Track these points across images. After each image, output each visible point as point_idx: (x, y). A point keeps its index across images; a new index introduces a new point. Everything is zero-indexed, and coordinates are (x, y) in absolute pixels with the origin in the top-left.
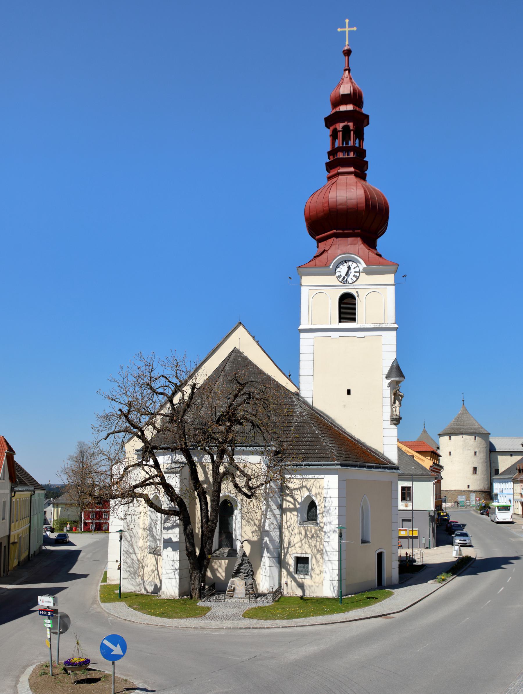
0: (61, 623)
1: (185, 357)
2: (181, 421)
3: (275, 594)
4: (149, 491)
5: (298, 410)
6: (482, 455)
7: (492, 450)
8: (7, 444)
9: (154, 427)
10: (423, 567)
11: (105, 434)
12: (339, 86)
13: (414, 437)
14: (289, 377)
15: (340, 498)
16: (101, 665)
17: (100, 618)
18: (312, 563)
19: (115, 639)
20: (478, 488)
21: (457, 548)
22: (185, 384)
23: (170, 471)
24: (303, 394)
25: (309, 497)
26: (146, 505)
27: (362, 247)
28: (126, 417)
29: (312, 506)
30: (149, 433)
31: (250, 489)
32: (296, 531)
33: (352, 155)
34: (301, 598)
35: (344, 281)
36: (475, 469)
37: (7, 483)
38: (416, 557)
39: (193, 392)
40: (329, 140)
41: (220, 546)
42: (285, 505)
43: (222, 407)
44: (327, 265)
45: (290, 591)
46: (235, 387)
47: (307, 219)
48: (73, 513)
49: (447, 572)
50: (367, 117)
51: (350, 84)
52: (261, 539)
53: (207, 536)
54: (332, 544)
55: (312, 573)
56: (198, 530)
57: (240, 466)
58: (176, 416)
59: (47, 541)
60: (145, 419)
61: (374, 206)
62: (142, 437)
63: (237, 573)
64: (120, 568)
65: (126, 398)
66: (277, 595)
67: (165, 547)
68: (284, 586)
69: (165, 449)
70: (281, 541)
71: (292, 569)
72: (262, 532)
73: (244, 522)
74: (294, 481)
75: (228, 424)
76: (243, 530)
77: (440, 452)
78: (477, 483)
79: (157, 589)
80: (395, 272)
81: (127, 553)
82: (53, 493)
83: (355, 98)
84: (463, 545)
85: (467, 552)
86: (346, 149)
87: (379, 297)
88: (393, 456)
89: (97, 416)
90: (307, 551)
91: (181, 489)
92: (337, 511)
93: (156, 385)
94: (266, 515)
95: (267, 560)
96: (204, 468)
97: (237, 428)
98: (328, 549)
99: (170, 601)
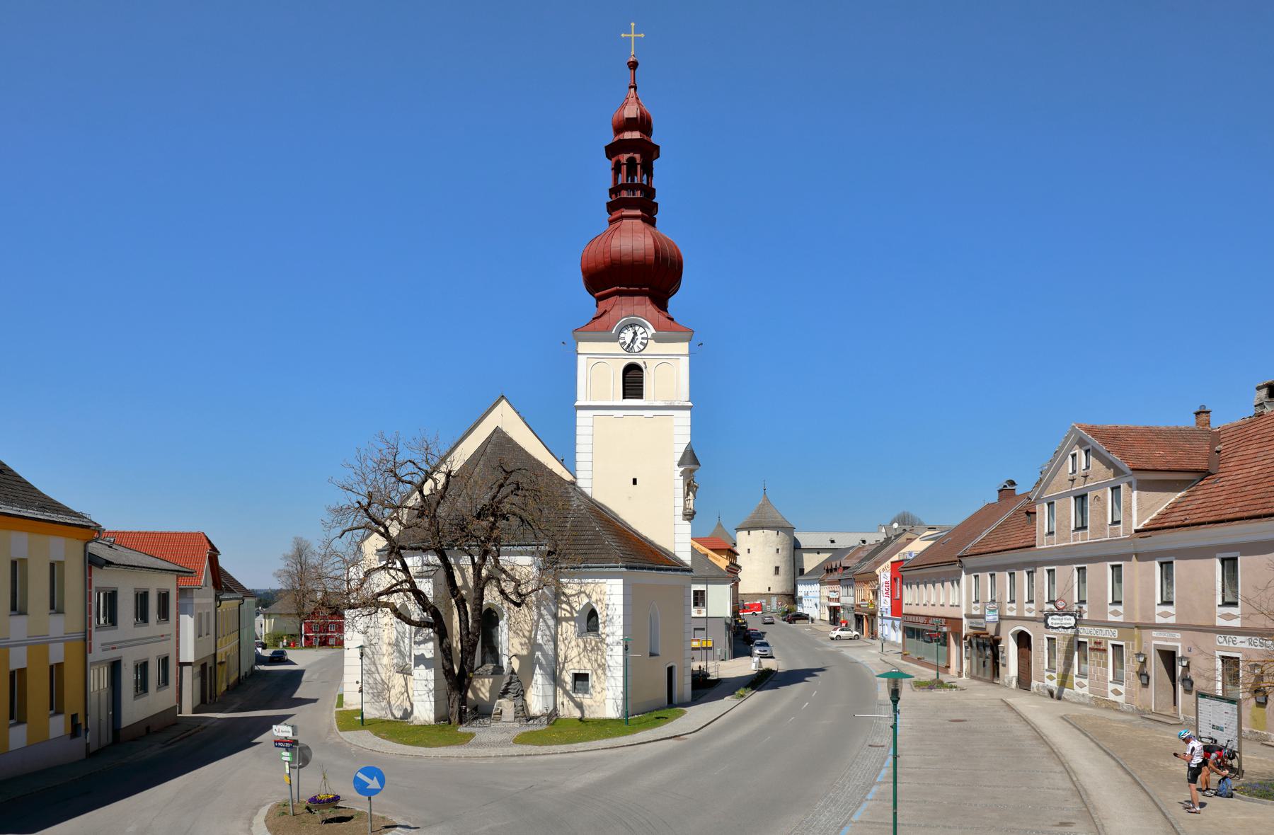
0: (300, 753)
1: (437, 438)
2: (434, 516)
3: (549, 716)
4: (397, 599)
5: (575, 503)
6: (784, 553)
7: (796, 547)
8: (209, 542)
9: (400, 523)
10: (718, 681)
11: (339, 531)
12: (623, 107)
13: (706, 534)
14: (562, 462)
15: (625, 605)
16: (353, 801)
17: (340, 749)
18: (593, 679)
19: (371, 772)
20: (779, 591)
21: (756, 659)
22: (436, 469)
23: (421, 575)
24: (581, 483)
25: (589, 604)
26: (392, 616)
27: (651, 309)
28: (366, 510)
29: (593, 614)
30: (394, 531)
31: (520, 595)
32: (573, 643)
33: (638, 194)
34: (580, 720)
35: (629, 349)
36: (777, 569)
37: (211, 591)
38: (711, 671)
39: (448, 482)
40: (611, 174)
41: (483, 663)
42: (562, 614)
43: (485, 499)
44: (609, 329)
45: (566, 712)
46: (501, 476)
47: (584, 272)
48: (291, 625)
49: (746, 687)
50: (657, 148)
51: (636, 106)
52: (532, 653)
53: (468, 651)
54: (615, 657)
55: (591, 690)
56: (456, 644)
57: (508, 568)
58: (426, 509)
59: (260, 660)
60: (387, 512)
61: (665, 259)
62: (386, 535)
63: (504, 693)
64: (361, 691)
65: (365, 488)
66: (552, 717)
67: (416, 665)
68: (559, 707)
69: (416, 549)
70: (556, 655)
71: (569, 687)
72: (533, 645)
73: (511, 634)
74: (571, 587)
75: (492, 519)
76: (509, 643)
77: (738, 550)
78: (778, 585)
79: (407, 714)
80: (689, 340)
81: (370, 673)
82: (265, 601)
83: (642, 123)
84: (763, 657)
85: (768, 664)
86: (632, 187)
87: (669, 370)
88: (685, 556)
89: (328, 509)
90: (586, 667)
91: (435, 597)
92: (621, 620)
93: (401, 472)
94: (537, 626)
95: (539, 677)
96: (462, 571)
97: (502, 523)
98: (610, 663)
99: (424, 727)
